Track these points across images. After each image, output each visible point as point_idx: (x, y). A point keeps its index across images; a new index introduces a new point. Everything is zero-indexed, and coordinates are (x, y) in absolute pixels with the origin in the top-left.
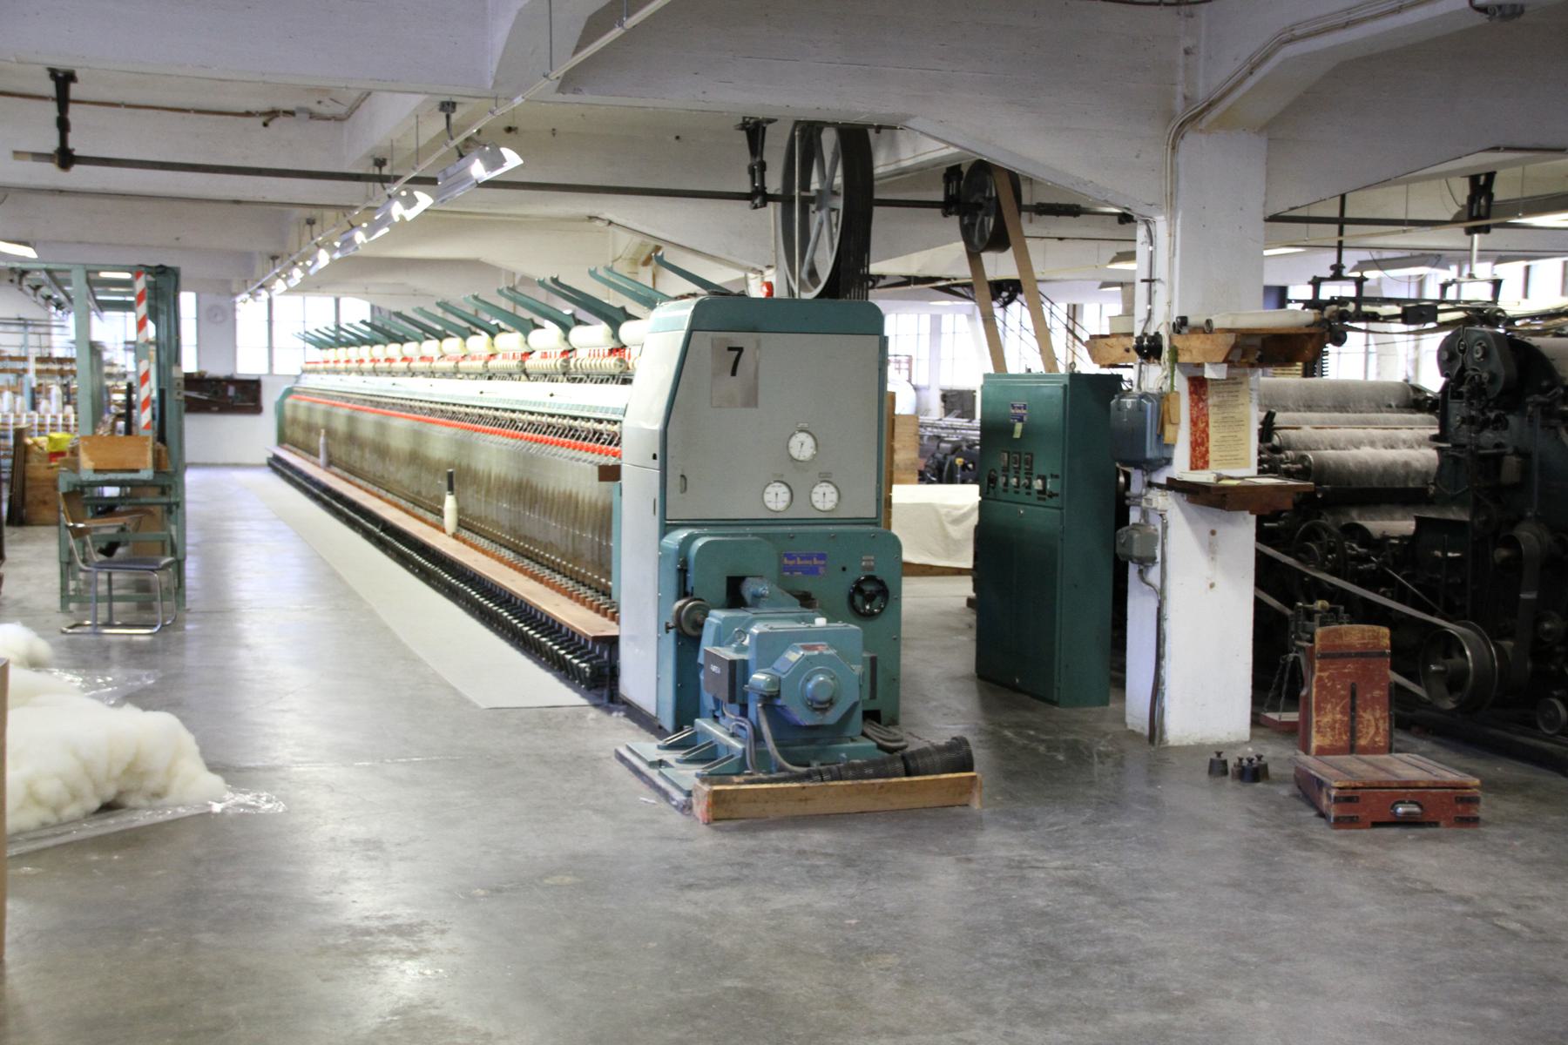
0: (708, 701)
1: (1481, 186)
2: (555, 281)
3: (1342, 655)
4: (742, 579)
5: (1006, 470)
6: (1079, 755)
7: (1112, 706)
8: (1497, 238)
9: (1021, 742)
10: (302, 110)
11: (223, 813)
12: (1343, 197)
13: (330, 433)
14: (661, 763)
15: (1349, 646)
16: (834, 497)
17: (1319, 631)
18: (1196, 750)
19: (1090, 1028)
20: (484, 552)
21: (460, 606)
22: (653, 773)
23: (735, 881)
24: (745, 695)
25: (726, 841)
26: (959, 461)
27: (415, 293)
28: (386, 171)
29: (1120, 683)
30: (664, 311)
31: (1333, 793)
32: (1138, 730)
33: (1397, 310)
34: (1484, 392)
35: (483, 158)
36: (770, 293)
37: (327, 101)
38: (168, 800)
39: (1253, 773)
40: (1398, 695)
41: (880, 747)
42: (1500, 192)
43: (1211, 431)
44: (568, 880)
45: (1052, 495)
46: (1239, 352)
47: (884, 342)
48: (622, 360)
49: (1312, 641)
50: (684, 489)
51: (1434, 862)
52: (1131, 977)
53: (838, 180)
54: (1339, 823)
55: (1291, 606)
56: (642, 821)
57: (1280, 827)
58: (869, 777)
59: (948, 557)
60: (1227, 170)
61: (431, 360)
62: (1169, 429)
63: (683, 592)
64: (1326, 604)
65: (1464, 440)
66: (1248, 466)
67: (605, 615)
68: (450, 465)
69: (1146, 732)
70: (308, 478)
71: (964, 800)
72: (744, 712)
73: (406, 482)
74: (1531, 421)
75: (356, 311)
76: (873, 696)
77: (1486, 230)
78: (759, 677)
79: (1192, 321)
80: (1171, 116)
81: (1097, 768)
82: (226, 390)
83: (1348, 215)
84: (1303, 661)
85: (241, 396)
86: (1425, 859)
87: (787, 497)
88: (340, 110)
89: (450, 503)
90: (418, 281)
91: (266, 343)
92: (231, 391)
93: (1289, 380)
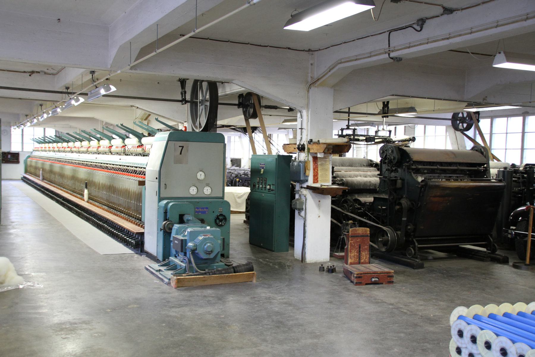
0: (173, 251)
1: (386, 105)
2: (122, 125)
3: (357, 236)
4: (184, 215)
5: (258, 183)
6: (282, 266)
7: (289, 252)
8: (390, 119)
9: (265, 263)
10: (42, 71)
11: (23, 288)
12: (349, 108)
13: (43, 170)
14: (160, 270)
15: (359, 234)
16: (210, 191)
17: (350, 229)
18: (315, 264)
19: (295, 345)
20: (98, 207)
21: (90, 223)
22: (157, 273)
23: (186, 305)
24: (186, 249)
25: (183, 293)
26: (238, 180)
27: (71, 127)
28: (69, 91)
29: (292, 246)
30: (159, 135)
31: (355, 275)
32: (298, 258)
33: (364, 138)
34: (392, 162)
35: (104, 88)
36: (186, 129)
37: (50, 69)
38: (4, 285)
39: (331, 270)
40: (372, 248)
41: (226, 265)
42: (391, 106)
43: (319, 172)
44: (135, 306)
45: (272, 190)
46: (327, 150)
47: (225, 145)
48: (143, 149)
49: (348, 232)
50: (166, 188)
51: (382, 294)
52: (305, 330)
53: (208, 97)
54: (357, 284)
55: (341, 223)
56: (155, 288)
57: (340, 285)
58: (223, 274)
59: (237, 208)
60: (323, 99)
61: (65, 148)
62: (307, 171)
63: (166, 219)
64: (352, 221)
65: (387, 175)
66: (329, 182)
67: (139, 226)
68: (86, 180)
69: (301, 259)
70: (36, 184)
71: (250, 280)
72: (185, 254)
73: (70, 185)
74: (404, 170)
75: (51, 133)
76: (223, 249)
77: (387, 117)
78: (190, 244)
79: (314, 140)
80: (307, 83)
81: (287, 270)
82: (7, 156)
83: (351, 111)
84: (345, 238)
85: (13, 158)
86: (381, 293)
87: (196, 190)
88: (55, 72)
89: (86, 192)
90: (73, 124)
91: (21, 142)
92: (9, 156)
93: (336, 157)
